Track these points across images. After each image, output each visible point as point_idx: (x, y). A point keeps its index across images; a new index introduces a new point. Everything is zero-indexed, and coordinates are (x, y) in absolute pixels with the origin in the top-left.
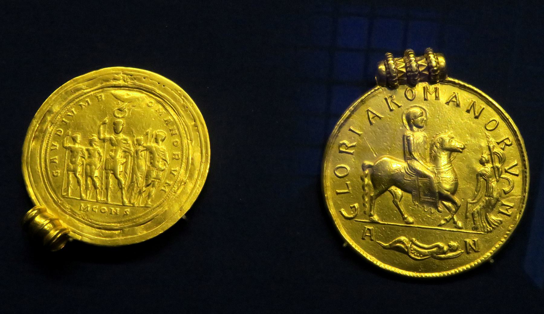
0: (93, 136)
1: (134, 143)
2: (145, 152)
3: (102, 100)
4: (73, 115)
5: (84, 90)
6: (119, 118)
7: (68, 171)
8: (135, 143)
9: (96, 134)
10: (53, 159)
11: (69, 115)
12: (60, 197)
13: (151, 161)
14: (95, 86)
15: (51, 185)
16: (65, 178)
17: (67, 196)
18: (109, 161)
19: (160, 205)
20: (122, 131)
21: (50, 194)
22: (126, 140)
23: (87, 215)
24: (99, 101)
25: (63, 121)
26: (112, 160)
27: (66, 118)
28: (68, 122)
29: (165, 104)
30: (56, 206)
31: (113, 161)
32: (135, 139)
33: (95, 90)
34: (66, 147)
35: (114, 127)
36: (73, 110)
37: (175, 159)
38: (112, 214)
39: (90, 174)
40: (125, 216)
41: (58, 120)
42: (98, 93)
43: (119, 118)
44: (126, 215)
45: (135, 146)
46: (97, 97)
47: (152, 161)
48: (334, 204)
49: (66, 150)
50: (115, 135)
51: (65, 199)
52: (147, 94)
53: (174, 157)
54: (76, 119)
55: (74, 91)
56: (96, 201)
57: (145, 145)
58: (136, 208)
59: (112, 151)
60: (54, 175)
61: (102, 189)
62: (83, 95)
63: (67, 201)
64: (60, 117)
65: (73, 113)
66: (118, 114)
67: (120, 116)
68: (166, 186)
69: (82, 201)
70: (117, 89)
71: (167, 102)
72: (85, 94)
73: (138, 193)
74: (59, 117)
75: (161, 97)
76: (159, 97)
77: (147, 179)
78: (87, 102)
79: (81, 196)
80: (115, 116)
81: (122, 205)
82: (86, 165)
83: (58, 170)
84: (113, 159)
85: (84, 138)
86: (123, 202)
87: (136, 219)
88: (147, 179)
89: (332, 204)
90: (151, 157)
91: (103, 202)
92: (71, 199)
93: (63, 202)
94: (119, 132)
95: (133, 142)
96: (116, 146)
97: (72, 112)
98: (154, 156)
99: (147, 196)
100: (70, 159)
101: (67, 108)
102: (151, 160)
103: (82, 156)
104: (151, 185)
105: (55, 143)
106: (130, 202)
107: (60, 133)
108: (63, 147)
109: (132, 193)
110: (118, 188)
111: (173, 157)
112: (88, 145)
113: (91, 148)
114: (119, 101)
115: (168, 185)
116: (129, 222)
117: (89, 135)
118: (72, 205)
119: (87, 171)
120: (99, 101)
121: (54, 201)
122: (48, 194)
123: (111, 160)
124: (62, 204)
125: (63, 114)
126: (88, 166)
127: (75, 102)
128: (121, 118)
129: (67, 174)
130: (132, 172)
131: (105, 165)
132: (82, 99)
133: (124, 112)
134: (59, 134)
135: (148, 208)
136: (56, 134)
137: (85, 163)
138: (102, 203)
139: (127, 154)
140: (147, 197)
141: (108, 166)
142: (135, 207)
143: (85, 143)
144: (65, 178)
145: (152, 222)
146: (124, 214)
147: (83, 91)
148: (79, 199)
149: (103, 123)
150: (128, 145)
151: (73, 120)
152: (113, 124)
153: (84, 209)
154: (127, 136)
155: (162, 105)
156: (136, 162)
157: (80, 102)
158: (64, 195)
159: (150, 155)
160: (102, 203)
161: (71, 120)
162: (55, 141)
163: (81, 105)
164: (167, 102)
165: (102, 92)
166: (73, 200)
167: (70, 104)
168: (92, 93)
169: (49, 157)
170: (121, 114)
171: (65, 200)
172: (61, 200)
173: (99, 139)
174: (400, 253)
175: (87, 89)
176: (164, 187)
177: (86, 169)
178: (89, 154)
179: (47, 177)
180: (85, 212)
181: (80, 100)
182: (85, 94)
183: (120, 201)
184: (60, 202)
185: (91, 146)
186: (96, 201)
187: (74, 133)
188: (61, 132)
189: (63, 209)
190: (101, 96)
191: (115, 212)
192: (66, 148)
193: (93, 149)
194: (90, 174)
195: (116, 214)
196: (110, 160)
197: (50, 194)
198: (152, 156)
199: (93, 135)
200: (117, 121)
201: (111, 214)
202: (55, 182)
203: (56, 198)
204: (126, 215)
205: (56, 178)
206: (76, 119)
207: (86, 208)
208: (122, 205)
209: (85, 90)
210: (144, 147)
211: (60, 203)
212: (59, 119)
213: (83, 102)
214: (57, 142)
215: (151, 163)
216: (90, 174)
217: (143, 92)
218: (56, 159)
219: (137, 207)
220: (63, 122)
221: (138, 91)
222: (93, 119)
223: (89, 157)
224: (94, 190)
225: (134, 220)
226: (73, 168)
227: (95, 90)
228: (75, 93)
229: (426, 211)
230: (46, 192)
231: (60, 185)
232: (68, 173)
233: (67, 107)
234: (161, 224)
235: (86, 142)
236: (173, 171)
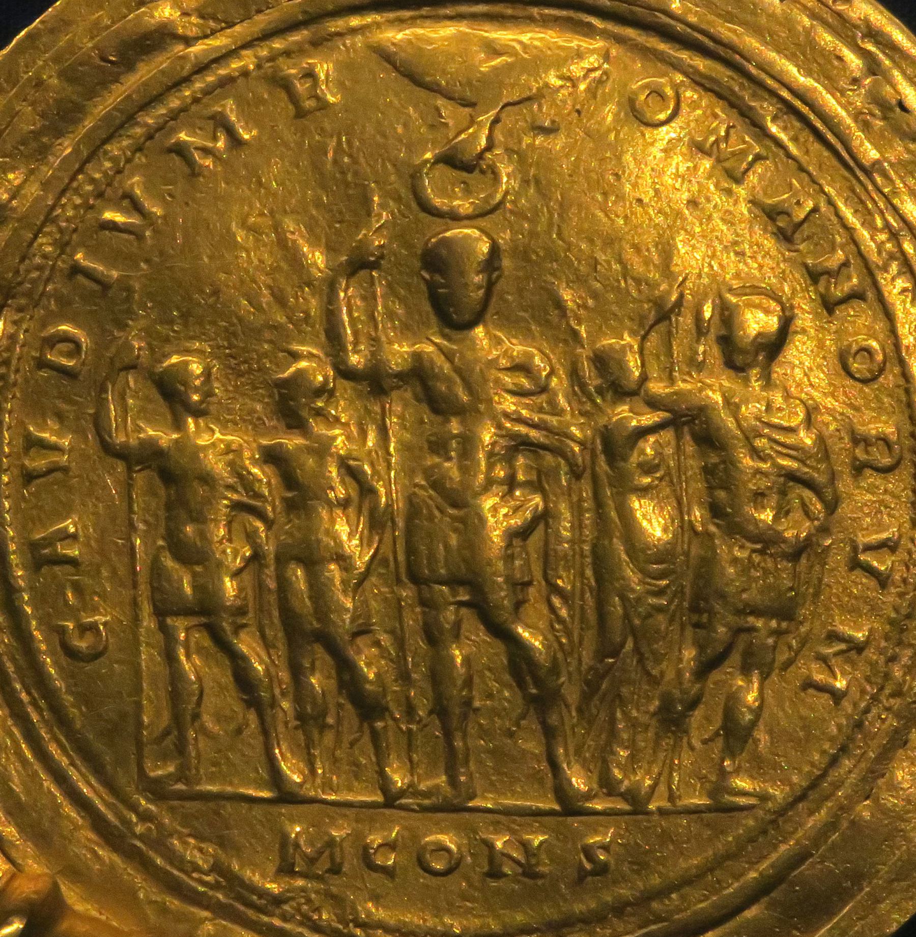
0: (295, 356)
1: (583, 386)
2: (667, 435)
3: (323, 105)
4: (134, 220)
5: (188, 41)
6: (455, 217)
7: (161, 613)
8: (592, 380)
9: (316, 345)
10: (49, 541)
11: (112, 226)
12: (130, 789)
13: (711, 495)
14: (259, 11)
15: (60, 718)
16: (149, 657)
17: (180, 786)
18: (431, 518)
19: (814, 784)
20: (491, 309)
21: (60, 778)
22: (522, 367)
23: (337, 900)
24: (301, 113)
25: (76, 270)
26: (451, 511)
27: (92, 252)
28: (115, 274)
29: (754, 96)
30: (117, 859)
31: (463, 520)
32: (584, 353)
33: (267, 36)
34: (125, 445)
35: (432, 288)
36: (136, 183)
37: (868, 472)
38: (506, 875)
39: (316, 625)
40: (589, 879)
41: (40, 268)
42: (287, 53)
43: (455, 217)
44: (594, 873)
45: (593, 402)
46: (285, 85)
47: (722, 494)
48: (779, 52)
49: (130, 469)
50: (445, 336)
51: (176, 803)
52: (620, 40)
53: (860, 453)
54: (161, 253)
55: (121, 54)
56: (379, 798)
57: (657, 387)
58: (656, 817)
59: (439, 446)
60: (71, 653)
61: (410, 711)
62: (187, 80)
63: (186, 820)
64: (54, 243)
65: (136, 207)
66: (443, 192)
67: (463, 205)
68: (836, 654)
69: (296, 809)
70: (413, 18)
72: (202, 68)
73: (654, 722)
74: (45, 245)
75: (721, 51)
76: (705, 52)
77: (705, 618)
78: (222, 124)
79: (276, 778)
80: (426, 207)
81: (557, 807)
82: (282, 560)
83: (95, 610)
84: (455, 505)
85: (240, 374)
86: (562, 791)
87: (662, 893)
88: (705, 618)
89: (774, 54)
90: (708, 471)
91: (427, 802)
92: (211, 805)
93: (160, 826)
94: (633, 386)
95: (574, 374)
96: (460, 411)
97: (126, 203)
98: (730, 463)
99: (717, 734)
100: (162, 530)
101: (93, 181)
102: (711, 488)
103: (245, 499)
104: (736, 658)
105: (43, 427)
106: (608, 786)
107: (69, 355)
108: (108, 449)
109: (613, 721)
110: (520, 701)
111: (855, 459)
112: (274, 423)
113: (292, 442)
114: (440, 102)
115: (843, 646)
116: (618, 918)
117: (265, 355)
118: (222, 842)
119: (295, 603)
120: (301, 113)
121: (98, 823)
122: (48, 784)
123: (442, 511)
124: (160, 843)
125: (68, 220)
126: (293, 565)
127: (138, 130)
128: (469, 217)
129: (160, 636)
130: (597, 581)
131: (410, 550)
132: (184, 109)
133: (483, 172)
134: (64, 361)
135: (736, 814)
136: (42, 364)
137: (270, 548)
138: (424, 809)
139: (549, 459)
140: (720, 743)
141: (432, 557)
142: (648, 813)
143: (252, 411)
144: (149, 657)
145: (772, 905)
146: (581, 867)
147: (179, 49)
148: (265, 794)
149: (350, 263)
150: (542, 399)
151: (147, 261)
152: (417, 264)
153: (312, 861)
154: (527, 335)
155: (732, 105)
156: (613, 514)
157: (174, 130)
158: (158, 781)
159: (703, 455)
160: (424, 809)
161: (130, 260)
162: (44, 417)
163: (180, 150)
165: (316, 43)
166: (228, 808)
167: (108, 147)
168: (247, 60)
169: (23, 529)
170: (468, 191)
171: (172, 809)
172: (145, 817)
173: (345, 373)
174: (638, 32)
175: (206, 37)
176: (823, 659)
177: (284, 585)
178: (289, 479)
179: (22, 662)
180: (319, 878)
181: (174, 115)
182: (202, 68)
183: (541, 782)
184: (139, 829)
185: (290, 427)
186: (379, 798)
187: (167, 349)
188: (78, 345)
189: (167, 873)
190: (310, 74)
191: (518, 863)
192: (122, 454)
193: (309, 450)
194: (319, 620)
195: (529, 872)
196: (437, 513)
197: (60, 778)
198: (714, 459)
199: (297, 347)
200: (446, 242)
201: (495, 873)
202: (85, 699)
203: (108, 805)
204: (594, 873)
205: (88, 667)
206: (161, 253)
207: (320, 853)
208: (557, 807)
209: (197, 39)
210: (653, 404)
211: (141, 837)
212: (45, 256)
213: (192, 129)
214: (60, 416)
215: (715, 511)
216: (316, 625)
217: (590, 25)
218: (66, 536)
219: (661, 812)
220: (80, 278)
221: (557, 19)
222: (282, 242)
223: (291, 506)
224: (361, 726)
225: (655, 905)
226: (194, 587)
227: (267, 36)
228: (130, 67)
230: (37, 767)
231: (123, 716)
232: (163, 628)
233: (89, 166)
234: (834, 914)
235: (259, 407)
236: (869, 548)
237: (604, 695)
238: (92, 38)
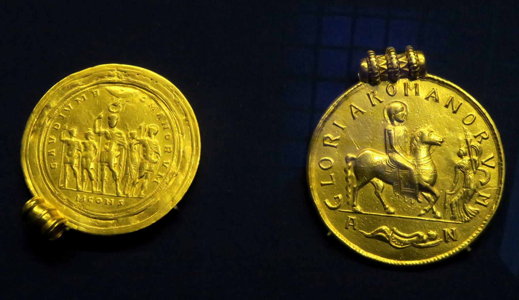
0: (89, 130)
1: (128, 137)
2: (139, 145)
3: (97, 95)
4: (69, 109)
5: (80, 86)
6: (113, 112)
7: (65, 163)
8: (129, 136)
9: (91, 128)
10: (50, 152)
11: (66, 110)
12: (57, 188)
13: (144, 154)
14: (90, 83)
15: (48, 177)
16: (62, 170)
17: (64, 188)
18: (104, 153)
19: (153, 196)
20: (116, 126)
21: (47, 185)
22: (120, 134)
23: (83, 206)
24: (94, 97)
25: (60, 115)
26: (107, 153)
27: (63, 113)
28: (65, 116)
29: (158, 99)
30: (53, 197)
31: (108, 154)
32: (129, 133)
33: (91, 86)
34: (63, 140)
35: (109, 122)
36: (70, 105)
37: (166, 152)
38: (107, 204)
39: (86, 167)
40: (119, 206)
41: (55, 115)
42: (93, 88)
43: (113, 112)
44: (120, 205)
45: (129, 139)
46: (93, 93)
47: (145, 154)
49: (63, 143)
50: (110, 129)
51: (62, 190)
52: (140, 90)
53: (166, 150)
54: (72, 114)
55: (70, 87)
56: (91, 192)
57: (138, 138)
58: (130, 198)
59: (107, 144)
60: (51, 168)
61: (97, 180)
62: (79, 91)
63: (64, 192)
64: (58, 112)
65: (70, 108)
66: (113, 109)
67: (115, 111)
68: (159, 178)
69: (78, 192)
70: (112, 85)
71: (160, 97)
72: (81, 89)
73: (132, 185)
74: (56, 112)
75: (154, 93)
76: (152, 93)
77: (140, 171)
78: (83, 97)
79: (77, 187)
80: (110, 111)
81: (116, 195)
82: (82, 157)
83: (55, 162)
84: (108, 152)
85: (80, 132)
86: (117, 193)
87: (129, 209)
88: (140, 171)
90: (144, 150)
91: (98, 193)
92: (68, 191)
93: (60, 193)
95: (127, 136)
96: (110, 139)
97: (68, 107)
98: (147, 149)
99: (140, 187)
100: (66, 152)
101: (64, 104)
102: (144, 153)
103: (78, 149)
104: (144, 177)
105: (52, 136)
106: (124, 193)
107: (57, 127)
108: (60, 140)
109: (126, 184)
110: (113, 180)
111: (165, 150)
112: (84, 139)
113: (86, 141)
114: (114, 97)
115: (160, 176)
116: (123, 212)
117: (85, 129)
118: (68, 196)
119: (83, 163)
120: (94, 97)
121: (52, 192)
122: (46, 186)
123: (106, 153)
124: (59, 195)
125: (60, 109)
126: (84, 158)
127: (71, 97)
128: (115, 113)
129: (64, 167)
130: (126, 164)
131: (100, 158)
132: (78, 95)
133: (118, 107)
134: (56, 128)
135: (142, 199)
136: (53, 128)
137: (81, 156)
138: (98, 194)
139: (122, 147)
140: (140, 189)
141: (103, 159)
142: (129, 197)
143: (81, 137)
144: (62, 170)
145: (145, 212)
146: (118, 204)
147: (79, 87)
148: (76, 190)
149: (98, 118)
150: (122, 138)
151: (70, 115)
152: (107, 118)
153: (80, 200)
154: (122, 130)
155: (154, 100)
156: (130, 155)
157: (76, 98)
158: (61, 187)
159: (143, 148)
160: (98, 194)
161: (68, 115)
162: (53, 135)
163: (77, 101)
164: (160, 97)
165: (97, 87)
166: (70, 191)
167: (67, 99)
168: (88, 89)
169: (47, 150)
170: (116, 109)
171: (62, 191)
172: (58, 191)
173: (95, 133)
174: (382, 242)
175: (83, 85)
176: (157, 178)
177: (82, 161)
178: (85, 147)
179: (44, 169)
180: (81, 202)
181: (76, 96)
182: (81, 89)
183: (114, 192)
184: (57, 193)
185: (86, 139)
186: (91, 192)
187: (71, 127)
188: (59, 126)
189: (60, 200)
190: (96, 92)
191: (110, 203)
192: (63, 141)
193: (89, 143)
194: (86, 166)
195: (111, 204)
196: (105, 153)
197: (47, 185)
198: (145, 149)
199: (89, 129)
200: (112, 116)
201: (106, 204)
202: (52, 174)
203: (53, 189)
204: (120, 205)
205: (53, 170)
206: (72, 114)
207: (82, 199)
208: (116, 195)
209: (81, 86)
210: (137, 140)
211: (57, 194)
212: (56, 113)
213: (79, 97)
214: (55, 135)
215: (144, 156)
216: (86, 167)
217: (136, 88)
218: (53, 152)
219: (131, 197)
220: (60, 117)
221: (132, 87)
222: (89, 114)
223: (85, 150)
224: (90, 182)
225: (128, 211)
226: (70, 160)
227: (91, 86)
228: (72, 89)
230: (44, 183)
231: (57, 177)
232: (65, 165)
233: (64, 102)
234: (154, 214)
235: (82, 136)
236: (165, 163)
237: (68, 176)
238: (390, 233)
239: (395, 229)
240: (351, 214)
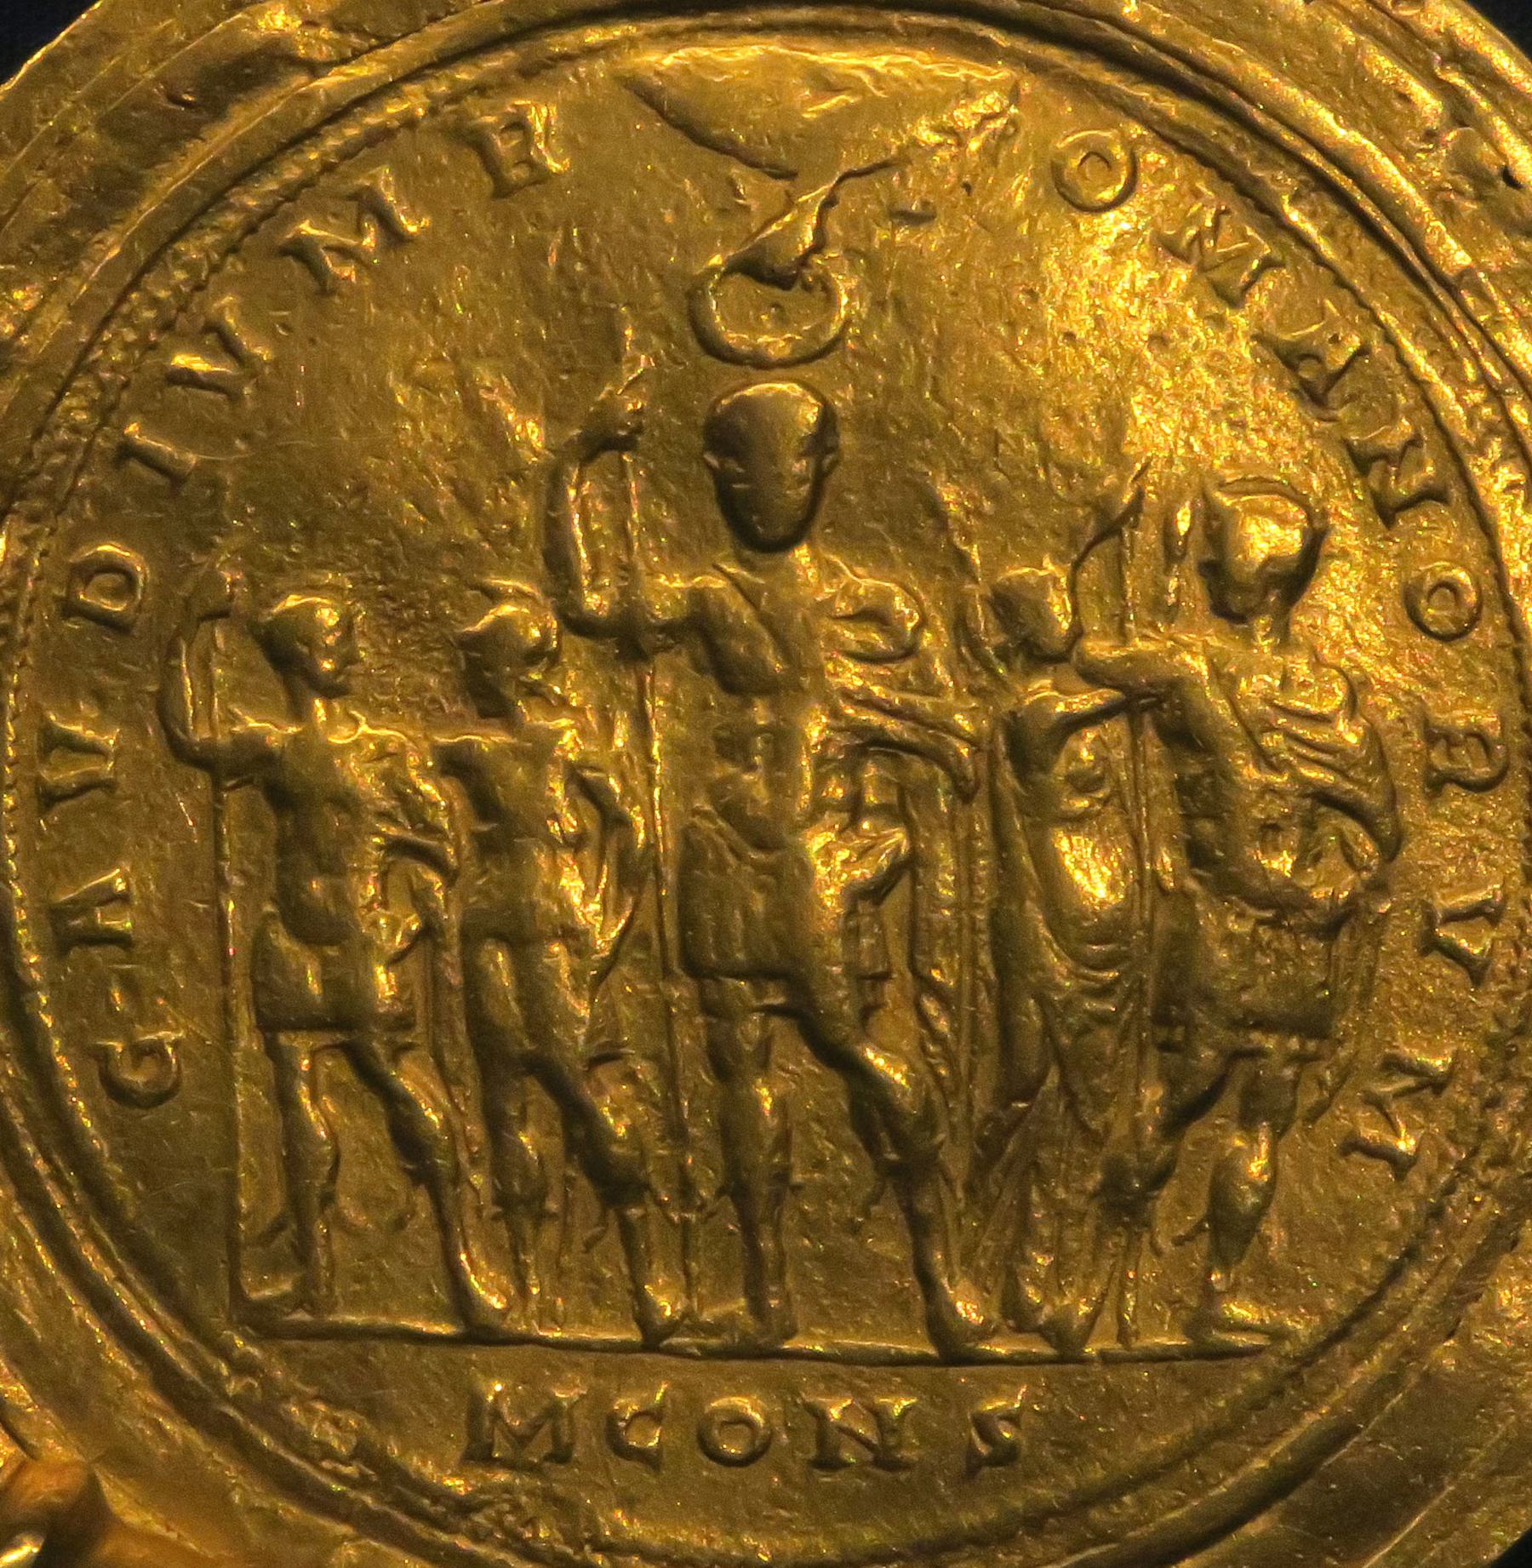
0: (494, 596)
1: (975, 646)
2: (1116, 729)
3: (541, 176)
4: (223, 368)
5: (314, 69)
6: (760, 364)
7: (269, 1025)
8: (991, 635)
9: (529, 578)
10: (82, 906)
11: (188, 379)
12: (218, 1321)
13: (1189, 829)
14: (433, 19)
15: (100, 1202)
16: (249, 1099)
17: (301, 1316)
18: (721, 866)
19: (1362, 1312)
20: (822, 518)
21: (101, 1302)
22: (873, 615)
23: (563, 1507)
24: (503, 190)
25: (127, 452)
26: (754, 855)
27: (154, 422)
28: (192, 458)
29: (1261, 160)
30: (195, 1437)
31: (774, 871)
32: (976, 591)
33: (447, 60)
34: (209, 745)
35: (722, 482)
36: (227, 307)
37: (1451, 789)
38: (846, 1465)
39: (528, 1045)
40: (986, 1470)
41: (66, 448)
42: (480, 89)
43: (760, 364)
44: (993, 1461)
45: (992, 672)
46: (477, 142)
47: (1207, 827)
49: (217, 785)
50: (743, 563)
51: (294, 1344)
52: (1036, 67)
53: (1438, 758)
54: (270, 424)
55: (203, 91)
56: (633, 1335)
57: (1099, 648)
58: (1097, 1368)
59: (733, 747)
60: (119, 1092)
61: (686, 1189)
62: (312, 134)
63: (311, 1372)
64: (91, 407)
65: (227, 346)
66: (740, 321)
67: (775, 344)
68: (1398, 1095)
69: (495, 1354)
70: (691, 31)
71: (1358, 195)
72: (337, 114)
73: (1093, 1208)
74: (76, 410)
75: (1206, 85)
76: (1179, 87)
77: (1179, 1034)
78: (371, 207)
79: (462, 1302)
80: (713, 347)
81: (931, 1351)
82: (471, 937)
83: (159, 1021)
84: (760, 846)
85: (402, 627)
86: (939, 1324)
87: (1107, 1494)
88: (1179, 1034)
90: (1184, 788)
91: (713, 1342)
92: (354, 1346)
93: (268, 1382)
94: (1059, 646)
95: (961, 626)
96: (770, 688)
97: (210, 339)
98: (1221, 774)
99: (1199, 1228)
100: (271, 888)
101: (155, 302)
102: (1188, 817)
103: (410, 836)
104: (1230, 1100)
105: (72, 715)
106: (1017, 1315)
107: (116, 594)
108: (180, 751)
109: (1025, 1206)
110: (870, 1173)
111: (1430, 767)
112: (458, 707)
113: (489, 739)
114: (736, 171)
115: (1410, 1082)
116: (1034, 1535)
117: (444, 594)
118: (372, 1410)
119: (494, 1010)
120: (503, 190)
121: (164, 1377)
122: (81, 1312)
123: (739, 856)
124: (267, 1411)
125: (113, 368)
126: (489, 946)
127: (231, 218)
128: (784, 364)
129: (267, 1065)
130: (998, 972)
131: (687, 921)
132: (307, 183)
133: (807, 288)
134: (108, 605)
135: (1230, 1362)
136: (70, 609)
137: (451, 918)
138: (709, 1354)
139: (918, 768)
140: (1204, 1243)
141: (722, 932)
142: (1084, 1361)
143: (422, 688)
144: (249, 1099)
145: (1291, 1515)
146: (972, 1451)
147: (299, 81)
148: (443, 1329)
149: (585, 439)
150: (907, 668)
151: (246, 437)
152: (698, 442)
153: (521, 1440)
154: (881, 561)
155: (1224, 176)
156: (1026, 860)
157: (291, 218)
158: (264, 1306)
159: (1175, 761)
160: (709, 1354)
161: (217, 436)
162: (73, 697)
163: (301, 251)
164: (1358, 195)
165: (529, 73)
166: (382, 1352)
167: (181, 246)
168: (414, 101)
169: (39, 885)
170: (782, 320)
171: (288, 1355)
172: (243, 1367)
173: (577, 624)
175: (345, 61)
176: (1377, 1104)
177: (474, 978)
178: (484, 802)
179: (36, 1108)
180: (533, 1470)
181: (291, 193)
182: (337, 114)
183: (905, 1308)
184: (232, 1388)
185: (484, 714)
186: (633, 1335)
187: (280, 583)
188: (130, 578)
189: (280, 1460)
190: (518, 125)
191: (866, 1443)
192: (204, 760)
193: (517, 753)
194: (533, 1037)
195: (884, 1459)
196: (730, 858)
197: (101, 1302)
198: (1194, 768)
199: (496, 581)
200: (745, 405)
201: (827, 1461)
202: (141, 1170)
203: (180, 1347)
204: (993, 1461)
205: (148, 1117)
206: (270, 424)
207: (536, 1427)
208: (931, 1351)
209: (330, 64)
210: (1093, 675)
211: (235, 1401)
212: (75, 429)
213: (321, 215)
214: (100, 697)
215: (1196, 854)
216: (528, 1045)
217: (986, 42)
218: (110, 898)
219: (1106, 1358)
220: (135, 466)
221: (931, 32)
222: (472, 405)
223: (487, 847)
224: (604, 1215)
225: (1095, 1514)
226: (325, 983)
227: (447, 60)
228: (218, 112)
229: (1051, 1520)
230: (62, 1283)
231: (206, 1198)
232: (273, 1051)
233: (149, 278)
234: (1395, 1530)
235: (433, 681)
236: (1453, 917)
239: (338, 143)
240: (1345, 454)
